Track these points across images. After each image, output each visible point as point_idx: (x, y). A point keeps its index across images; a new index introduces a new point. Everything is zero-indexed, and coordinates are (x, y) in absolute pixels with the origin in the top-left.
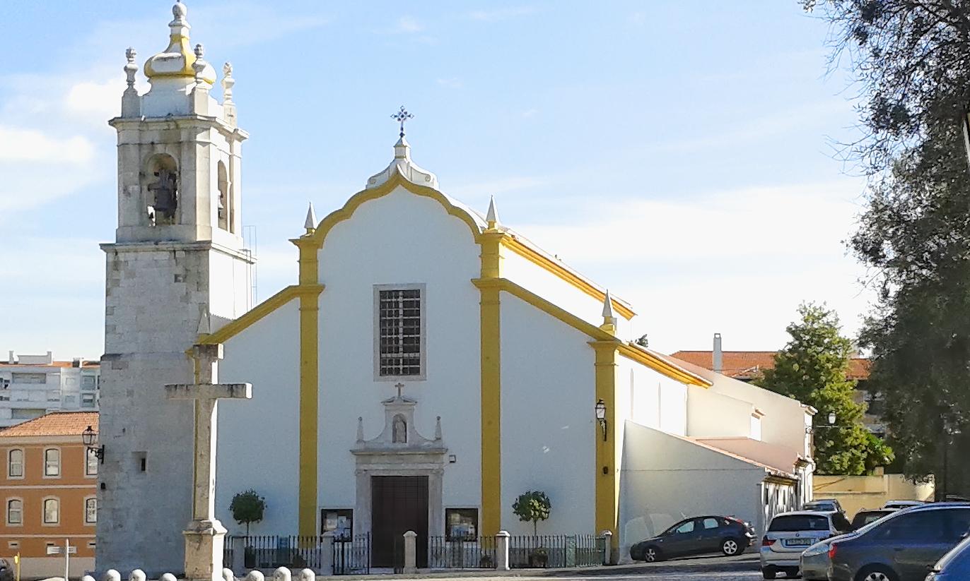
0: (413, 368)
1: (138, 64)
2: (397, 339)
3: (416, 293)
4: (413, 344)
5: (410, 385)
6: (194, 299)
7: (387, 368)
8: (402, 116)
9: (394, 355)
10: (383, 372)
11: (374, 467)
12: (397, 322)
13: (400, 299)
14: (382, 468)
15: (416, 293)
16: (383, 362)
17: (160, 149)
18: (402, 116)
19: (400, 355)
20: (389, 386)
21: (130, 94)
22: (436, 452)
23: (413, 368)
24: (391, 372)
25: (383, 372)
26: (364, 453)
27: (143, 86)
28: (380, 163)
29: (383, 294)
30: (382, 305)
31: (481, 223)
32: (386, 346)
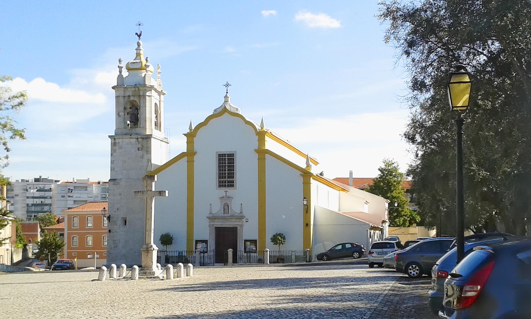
0: (231, 184)
1: (123, 64)
2: (225, 173)
3: (232, 155)
4: (231, 175)
5: (230, 191)
6: (145, 157)
7: (221, 185)
8: (227, 85)
9: (224, 179)
10: (220, 186)
11: (216, 223)
12: (225, 166)
13: (226, 157)
14: (219, 224)
15: (232, 155)
16: (220, 182)
17: (132, 98)
18: (227, 85)
19: (226, 179)
20: (222, 192)
21: (120, 77)
22: (241, 217)
23: (231, 184)
24: (223, 186)
25: (220, 186)
26: (212, 218)
27: (125, 73)
28: (218, 103)
29: (220, 155)
30: (219, 160)
31: (258, 127)
32: (221, 176)
